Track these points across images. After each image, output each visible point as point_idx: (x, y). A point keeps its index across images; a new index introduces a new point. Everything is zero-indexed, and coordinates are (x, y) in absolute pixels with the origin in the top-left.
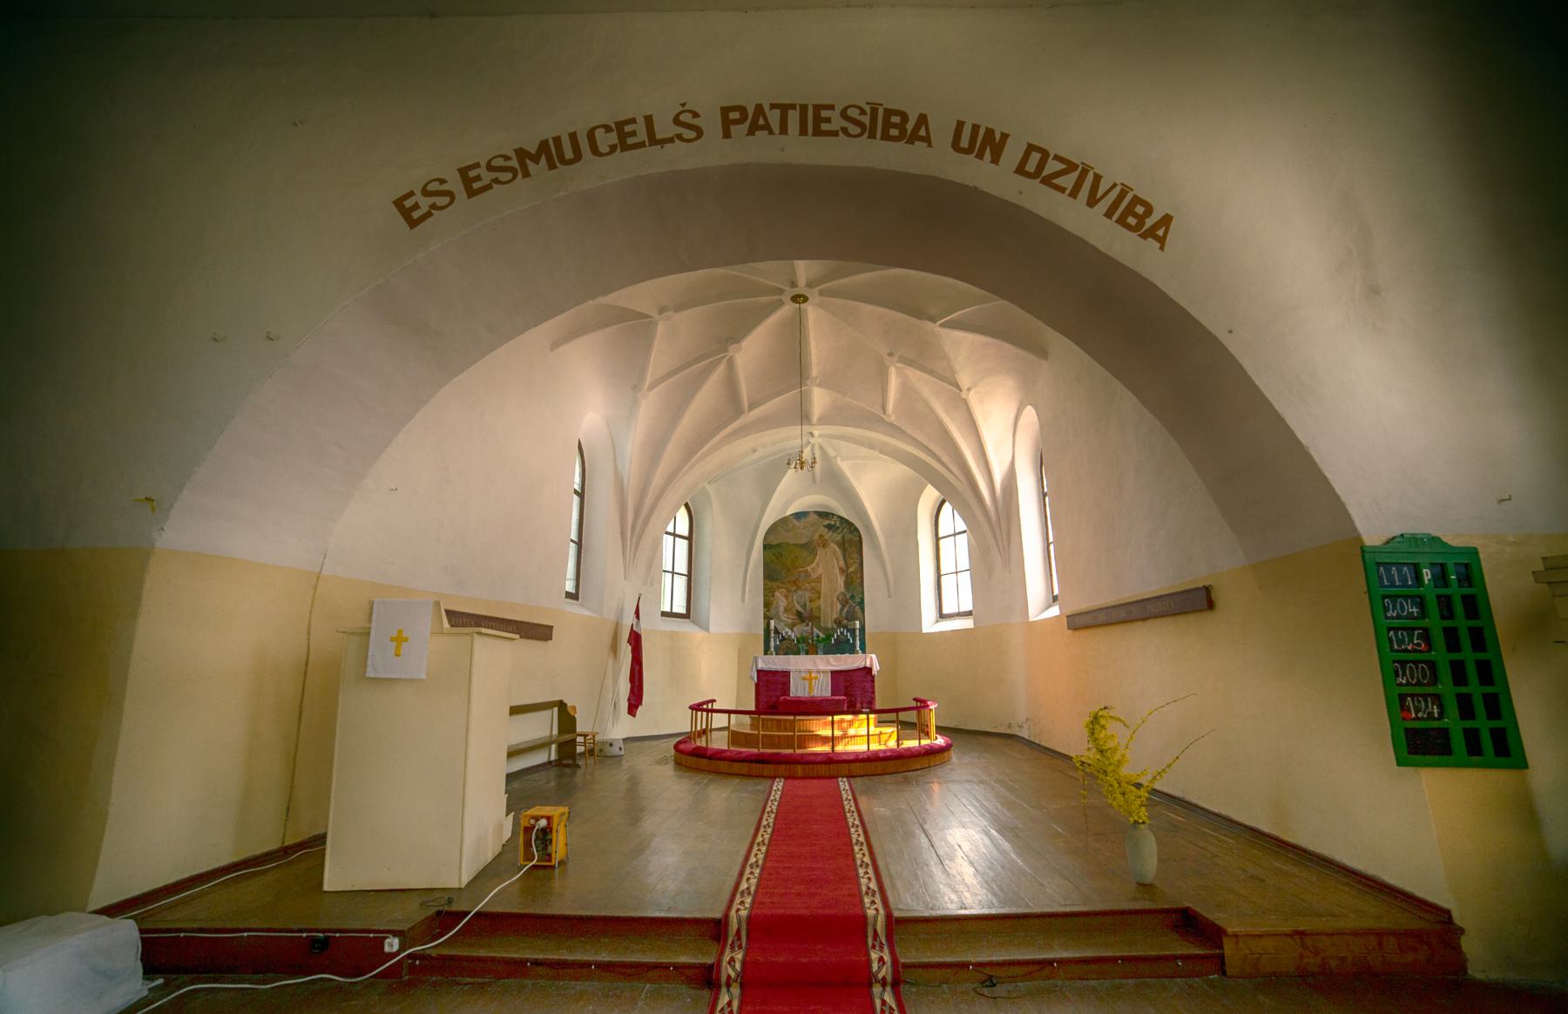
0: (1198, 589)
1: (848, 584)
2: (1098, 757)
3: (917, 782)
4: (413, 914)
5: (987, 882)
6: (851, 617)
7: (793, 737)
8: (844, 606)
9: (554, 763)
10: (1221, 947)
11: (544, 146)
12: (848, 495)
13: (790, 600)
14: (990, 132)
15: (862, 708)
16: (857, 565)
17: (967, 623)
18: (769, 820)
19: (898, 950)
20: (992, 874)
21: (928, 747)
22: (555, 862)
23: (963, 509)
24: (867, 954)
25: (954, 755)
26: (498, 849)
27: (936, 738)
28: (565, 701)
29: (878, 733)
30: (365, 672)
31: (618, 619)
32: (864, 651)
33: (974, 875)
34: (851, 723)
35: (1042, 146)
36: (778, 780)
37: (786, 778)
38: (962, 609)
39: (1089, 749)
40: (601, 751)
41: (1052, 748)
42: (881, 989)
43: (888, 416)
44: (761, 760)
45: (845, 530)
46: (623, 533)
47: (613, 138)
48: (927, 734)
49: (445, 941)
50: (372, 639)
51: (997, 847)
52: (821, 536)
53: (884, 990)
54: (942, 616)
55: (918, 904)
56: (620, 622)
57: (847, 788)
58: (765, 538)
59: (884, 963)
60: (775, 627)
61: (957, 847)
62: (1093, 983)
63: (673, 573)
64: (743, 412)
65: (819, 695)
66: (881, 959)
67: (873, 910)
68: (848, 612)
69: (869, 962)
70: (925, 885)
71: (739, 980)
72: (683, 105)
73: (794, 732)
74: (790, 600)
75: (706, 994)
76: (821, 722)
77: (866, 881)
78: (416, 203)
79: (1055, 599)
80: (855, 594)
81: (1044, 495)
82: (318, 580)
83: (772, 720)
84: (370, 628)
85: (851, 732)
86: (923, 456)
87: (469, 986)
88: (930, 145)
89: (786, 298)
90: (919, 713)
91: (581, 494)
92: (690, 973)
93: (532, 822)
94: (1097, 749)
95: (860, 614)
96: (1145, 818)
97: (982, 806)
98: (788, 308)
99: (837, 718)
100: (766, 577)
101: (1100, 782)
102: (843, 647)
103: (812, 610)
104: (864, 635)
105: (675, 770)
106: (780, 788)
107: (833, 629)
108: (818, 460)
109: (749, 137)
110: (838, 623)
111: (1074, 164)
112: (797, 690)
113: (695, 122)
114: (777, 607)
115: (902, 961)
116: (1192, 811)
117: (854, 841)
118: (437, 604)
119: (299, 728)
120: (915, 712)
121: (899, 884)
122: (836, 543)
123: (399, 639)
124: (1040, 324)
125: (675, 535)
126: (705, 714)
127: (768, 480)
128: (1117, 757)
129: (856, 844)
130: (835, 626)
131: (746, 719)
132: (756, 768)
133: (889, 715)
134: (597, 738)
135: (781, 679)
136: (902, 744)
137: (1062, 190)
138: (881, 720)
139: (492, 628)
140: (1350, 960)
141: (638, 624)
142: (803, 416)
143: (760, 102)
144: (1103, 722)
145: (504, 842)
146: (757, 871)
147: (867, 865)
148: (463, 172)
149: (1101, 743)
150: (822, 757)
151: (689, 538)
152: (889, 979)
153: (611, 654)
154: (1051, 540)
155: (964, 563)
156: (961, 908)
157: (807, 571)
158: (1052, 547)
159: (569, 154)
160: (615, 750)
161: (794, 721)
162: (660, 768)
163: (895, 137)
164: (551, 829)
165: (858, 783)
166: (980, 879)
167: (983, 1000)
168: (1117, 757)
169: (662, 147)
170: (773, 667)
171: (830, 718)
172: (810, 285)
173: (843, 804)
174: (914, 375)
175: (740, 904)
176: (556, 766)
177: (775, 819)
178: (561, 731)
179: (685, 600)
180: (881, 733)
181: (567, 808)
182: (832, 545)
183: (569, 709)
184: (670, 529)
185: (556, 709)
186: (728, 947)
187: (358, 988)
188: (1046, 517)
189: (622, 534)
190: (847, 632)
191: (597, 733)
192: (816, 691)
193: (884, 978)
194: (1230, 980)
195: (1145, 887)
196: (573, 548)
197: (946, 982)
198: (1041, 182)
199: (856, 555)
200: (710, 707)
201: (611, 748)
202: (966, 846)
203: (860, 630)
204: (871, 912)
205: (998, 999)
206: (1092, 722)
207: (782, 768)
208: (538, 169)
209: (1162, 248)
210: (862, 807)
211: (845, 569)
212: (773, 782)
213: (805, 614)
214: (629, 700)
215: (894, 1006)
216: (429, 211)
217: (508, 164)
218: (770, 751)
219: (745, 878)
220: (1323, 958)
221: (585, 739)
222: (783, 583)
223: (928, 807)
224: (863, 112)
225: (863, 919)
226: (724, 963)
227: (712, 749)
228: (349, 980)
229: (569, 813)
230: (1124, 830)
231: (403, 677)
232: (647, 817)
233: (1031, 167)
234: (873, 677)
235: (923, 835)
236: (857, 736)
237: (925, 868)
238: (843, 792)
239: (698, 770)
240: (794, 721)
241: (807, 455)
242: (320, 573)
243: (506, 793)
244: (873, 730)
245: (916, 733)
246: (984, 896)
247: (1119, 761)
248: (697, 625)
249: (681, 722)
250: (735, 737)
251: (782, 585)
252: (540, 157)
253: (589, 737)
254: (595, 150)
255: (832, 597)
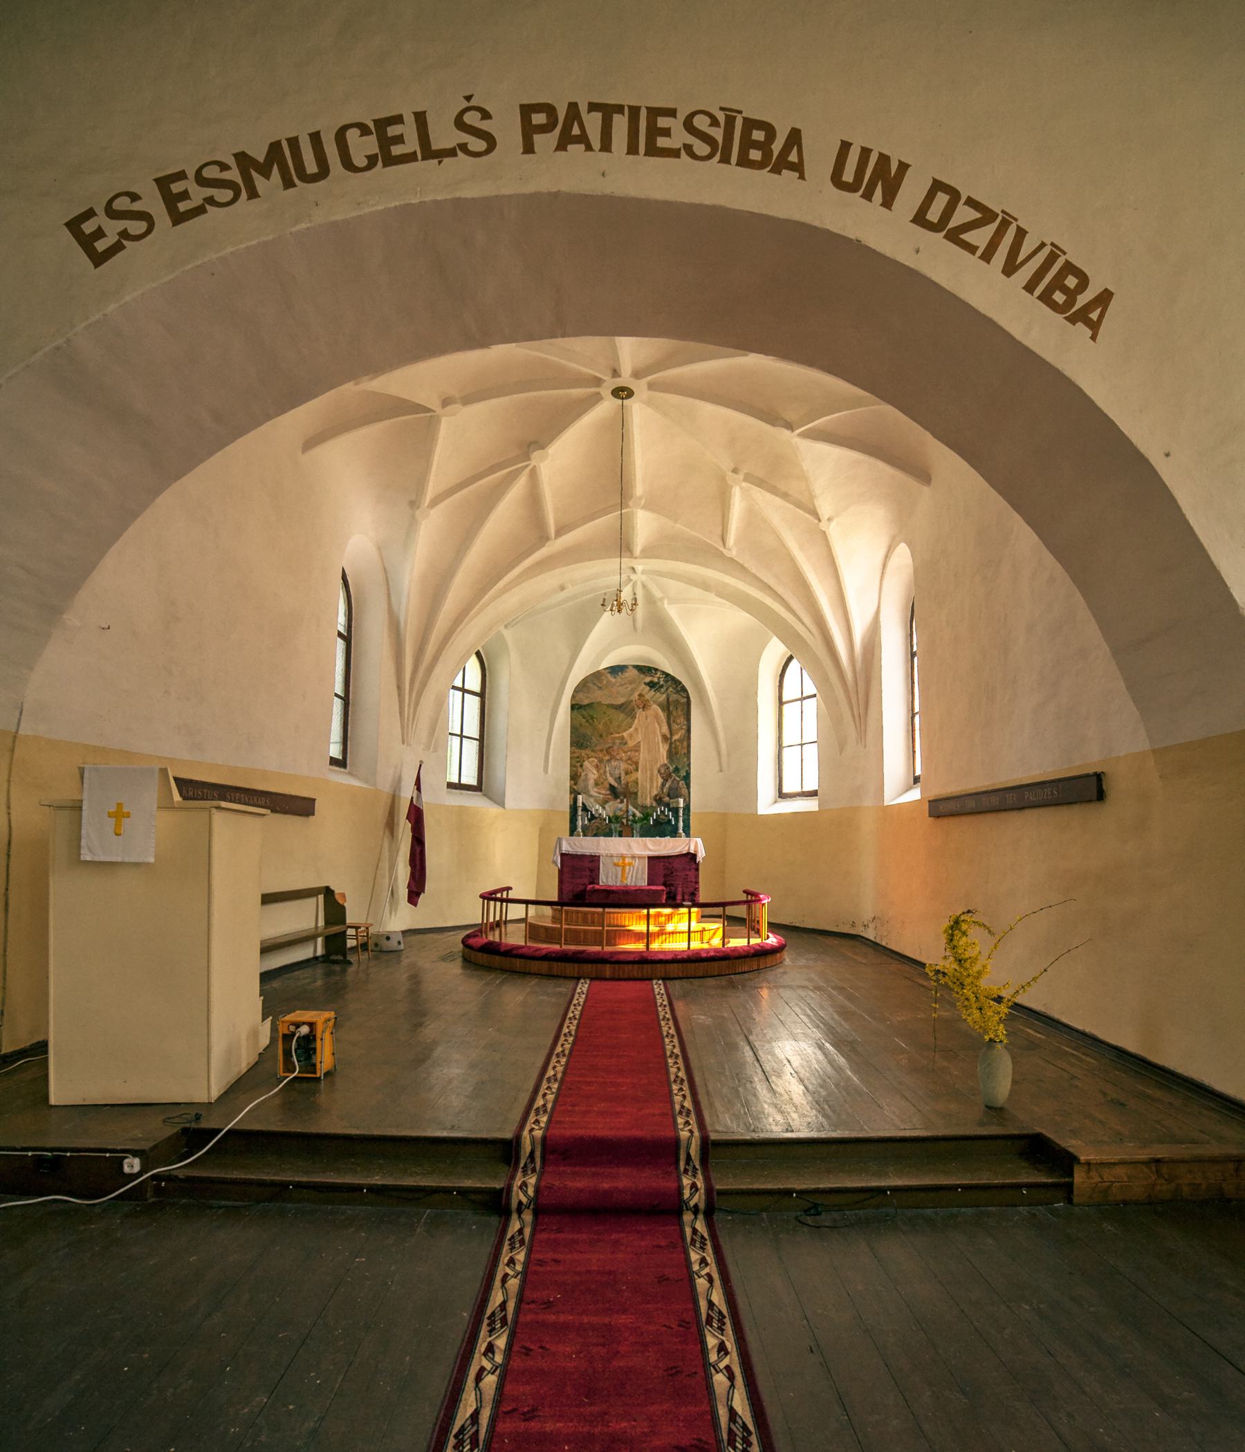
0: (1087, 776)
1: (671, 754)
2: (955, 966)
3: (744, 986)
4: (159, 1131)
5: (817, 1102)
6: (674, 793)
7: (601, 933)
8: (666, 780)
9: (321, 959)
10: (1071, 1175)
11: (275, 147)
12: (675, 645)
13: (602, 771)
14: (884, 159)
15: (684, 900)
16: (683, 731)
17: (811, 805)
18: (570, 1027)
19: (713, 1175)
20: (824, 1093)
21: (758, 948)
22: (320, 1073)
23: (814, 667)
24: (679, 1180)
25: (787, 957)
26: (254, 1058)
27: (768, 937)
28: (332, 888)
29: (700, 929)
30: (79, 854)
31: (394, 792)
32: (688, 835)
33: (804, 1094)
34: (670, 917)
35: (952, 184)
36: (582, 981)
37: (592, 979)
38: (807, 788)
39: (945, 958)
40: (376, 945)
41: (901, 952)
42: (693, 1217)
43: (730, 550)
44: (564, 957)
45: (671, 689)
46: (400, 688)
47: (371, 145)
48: (758, 932)
49: (194, 1161)
50: (85, 813)
51: (831, 1062)
52: (640, 695)
53: (696, 1218)
54: (782, 795)
55: (738, 1126)
56: (396, 794)
57: (663, 991)
58: (573, 697)
59: (697, 1190)
60: (583, 804)
61: (785, 1062)
62: (929, 1211)
63: (461, 736)
64: (548, 539)
65: (633, 884)
66: (694, 1186)
67: (687, 1131)
68: (670, 788)
69: (680, 1189)
70: (747, 1104)
71: (531, 1207)
72: (468, 98)
73: (603, 928)
74: (602, 771)
75: (494, 1220)
76: (635, 916)
77: (681, 1098)
78: (100, 228)
79: (916, 780)
80: (680, 767)
81: (913, 655)
82: (14, 742)
83: (577, 912)
84: (82, 801)
85: (670, 927)
86: (769, 601)
87: (223, 1209)
88: (802, 177)
89: (606, 391)
90: (749, 908)
91: (347, 639)
92: (479, 1197)
93: (292, 1028)
94: (956, 958)
95: (684, 791)
96: (1002, 1037)
97: (816, 1014)
98: (608, 405)
99: (652, 911)
100: (573, 744)
101: (955, 995)
102: (662, 828)
103: (628, 783)
104: (689, 816)
105: (464, 967)
106: (585, 990)
107: (651, 806)
108: (640, 601)
109: (558, 153)
110: (658, 800)
111: (991, 211)
112: (608, 878)
113: (484, 125)
114: (586, 780)
115: (718, 1187)
116: (1051, 1026)
117: (668, 1053)
118: (164, 772)
119: (6, 922)
120: (745, 907)
121: (718, 1105)
122: (660, 705)
123: (119, 815)
124: (928, 436)
125: (464, 690)
126: (498, 904)
127: (579, 627)
128: (977, 968)
129: (671, 1056)
130: (654, 804)
131: (548, 911)
132: (557, 967)
133: (715, 909)
134: (371, 930)
135: (587, 864)
136: (729, 942)
137: (971, 249)
138: (705, 914)
139: (240, 802)
140: (1203, 1187)
141: (419, 797)
142: (622, 544)
143: (574, 101)
144: (964, 927)
145: (261, 1051)
146: (555, 1086)
147: (682, 1080)
148: (163, 183)
149: (960, 952)
150: (636, 955)
151: (482, 695)
152: (702, 1206)
153: (387, 832)
154: (917, 709)
155: (811, 734)
156: (787, 1131)
157: (623, 738)
158: (917, 718)
159: (311, 167)
160: (393, 944)
161: (603, 914)
162: (443, 966)
163: (754, 162)
164: (314, 1036)
165: (676, 986)
166: (810, 1098)
167: (806, 1229)
168: (977, 968)
169: (440, 162)
170: (580, 851)
171: (645, 911)
172: (637, 375)
173: (657, 1010)
174: (763, 499)
175: (534, 1123)
176: (323, 962)
177: (578, 1026)
178: (328, 922)
179: (477, 762)
180: (704, 930)
181: (333, 1013)
182: (655, 706)
183: (337, 897)
184: (458, 683)
185: (321, 897)
186: (520, 1170)
187: (97, 1210)
188: (913, 683)
189: (399, 688)
190: (669, 811)
191: (372, 925)
192: (629, 880)
193: (696, 1206)
194: (1076, 1208)
195: (995, 1111)
196: (338, 705)
197: (765, 1210)
198: (946, 237)
199: (682, 720)
200: (505, 896)
201: (389, 942)
202: (796, 1062)
203: (684, 809)
204: (684, 1134)
205: (822, 1229)
206: (952, 928)
207: (588, 968)
208: (269, 185)
209: (1093, 338)
210: (679, 1014)
211: (669, 736)
212: (577, 985)
213: (620, 789)
214: (409, 886)
215: (706, 1235)
216: (119, 242)
217: (226, 175)
218: (573, 948)
219: (541, 1093)
220: (1178, 1185)
221: (357, 932)
222: (593, 751)
223: (755, 1015)
224: (714, 122)
225: (675, 1143)
226: (515, 1188)
227: (506, 945)
228: (86, 1202)
229: (336, 1018)
230: (981, 1046)
231: (127, 860)
232: (428, 1023)
233: (934, 215)
234: (698, 865)
235: (747, 1048)
236: (676, 933)
237: (748, 1085)
238: (658, 997)
239: (489, 968)
240: (603, 914)
241: (626, 595)
242: (17, 733)
243: (260, 996)
244: (695, 926)
245: (744, 930)
246: (814, 1118)
247: (979, 973)
248: (490, 799)
249: (471, 913)
250: (534, 931)
251: (593, 754)
252: (271, 167)
253: (362, 929)
254: (348, 164)
255: (651, 771)
